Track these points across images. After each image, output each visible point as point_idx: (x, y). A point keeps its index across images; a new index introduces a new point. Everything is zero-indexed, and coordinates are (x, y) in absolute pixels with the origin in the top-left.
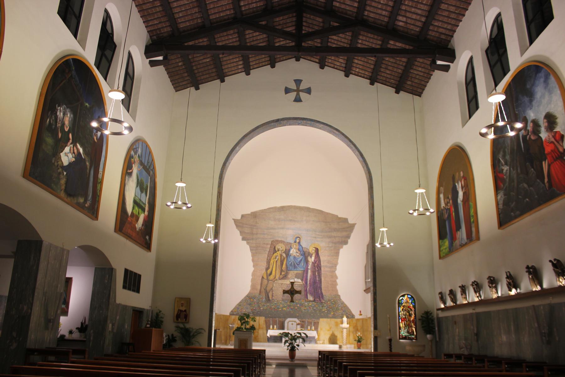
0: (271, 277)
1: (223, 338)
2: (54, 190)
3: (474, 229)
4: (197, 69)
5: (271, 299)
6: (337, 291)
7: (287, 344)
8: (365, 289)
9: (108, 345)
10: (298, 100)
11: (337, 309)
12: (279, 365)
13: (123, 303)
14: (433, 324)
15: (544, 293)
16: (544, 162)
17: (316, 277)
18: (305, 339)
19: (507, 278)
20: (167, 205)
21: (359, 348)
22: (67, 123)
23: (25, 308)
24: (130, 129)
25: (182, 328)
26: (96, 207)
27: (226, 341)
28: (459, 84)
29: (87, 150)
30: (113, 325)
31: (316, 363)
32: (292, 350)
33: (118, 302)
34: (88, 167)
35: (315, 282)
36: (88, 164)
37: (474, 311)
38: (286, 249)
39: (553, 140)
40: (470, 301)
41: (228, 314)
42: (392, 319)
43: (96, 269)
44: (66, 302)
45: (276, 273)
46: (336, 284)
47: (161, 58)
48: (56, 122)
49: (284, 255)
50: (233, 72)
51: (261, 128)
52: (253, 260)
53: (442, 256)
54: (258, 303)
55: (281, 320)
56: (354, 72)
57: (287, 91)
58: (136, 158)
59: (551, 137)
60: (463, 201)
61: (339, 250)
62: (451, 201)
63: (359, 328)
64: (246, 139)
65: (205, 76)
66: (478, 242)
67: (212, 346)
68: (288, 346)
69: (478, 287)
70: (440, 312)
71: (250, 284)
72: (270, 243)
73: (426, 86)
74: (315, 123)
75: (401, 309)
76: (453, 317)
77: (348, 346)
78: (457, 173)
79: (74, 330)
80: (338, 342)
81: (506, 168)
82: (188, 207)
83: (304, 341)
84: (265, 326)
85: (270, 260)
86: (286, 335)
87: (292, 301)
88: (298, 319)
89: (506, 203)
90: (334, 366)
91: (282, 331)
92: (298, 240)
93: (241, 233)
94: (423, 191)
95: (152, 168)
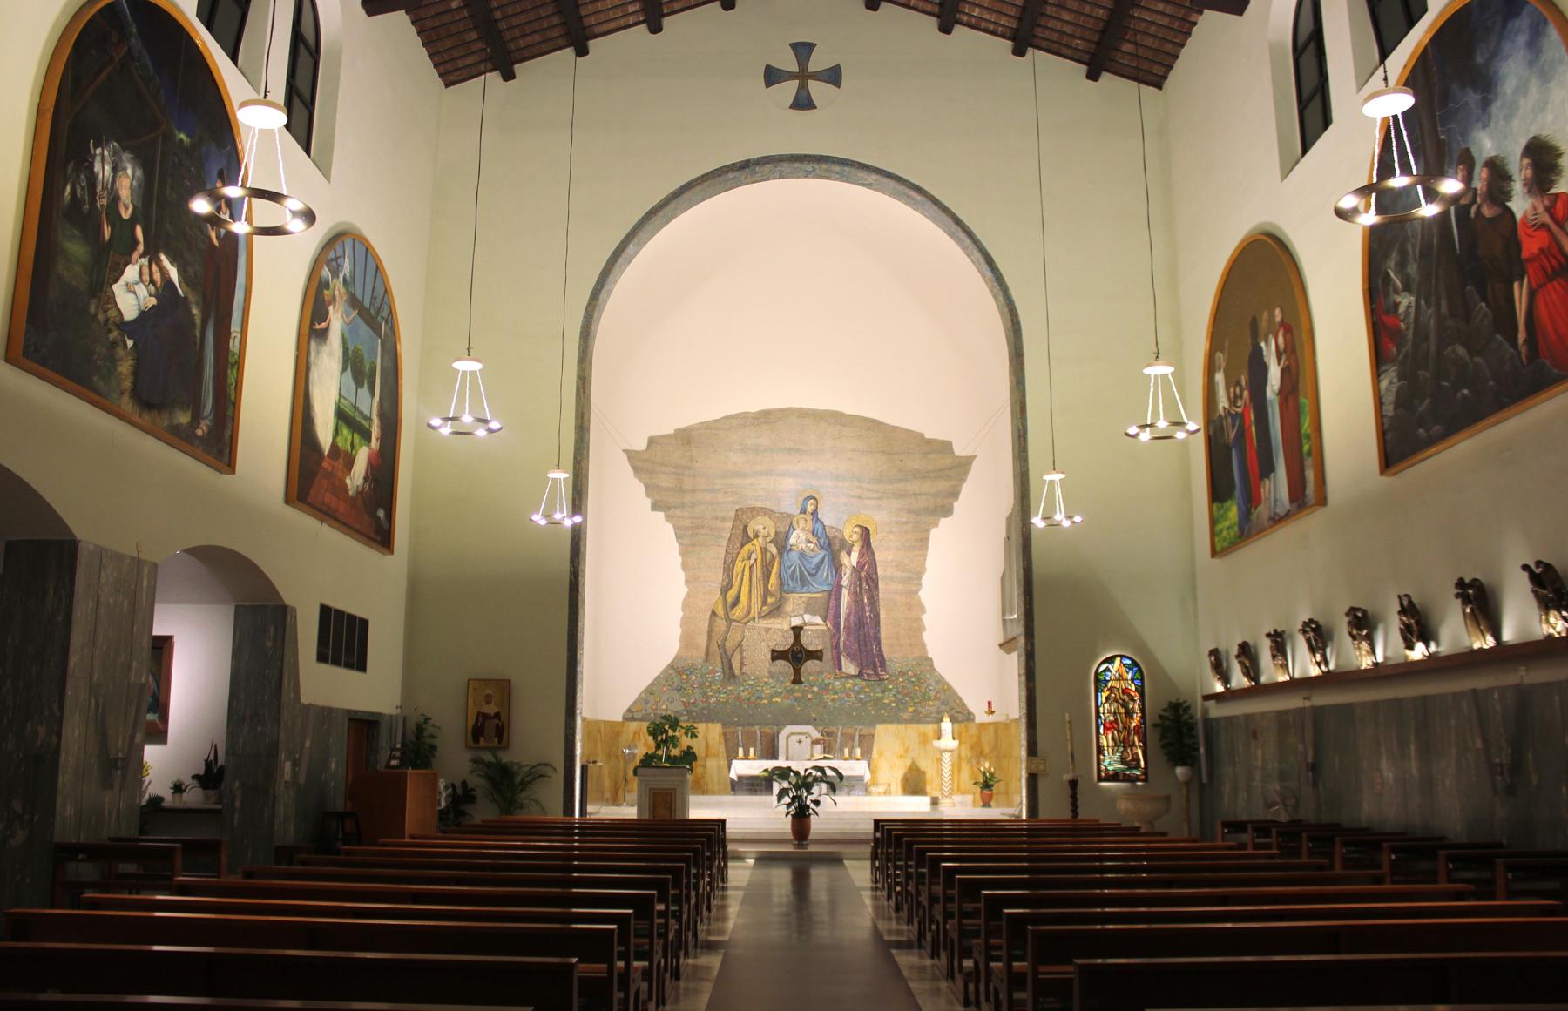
0: (738, 612)
1: (607, 783)
2: (100, 394)
3: (1310, 474)
4: (506, 17)
5: (737, 672)
6: (924, 645)
7: (787, 800)
8: (1001, 641)
9: (286, 824)
10: (803, 102)
11: (924, 698)
12: (765, 859)
14: (1194, 737)
15: (1504, 655)
16: (1516, 285)
17: (863, 609)
18: (836, 783)
19: (1403, 611)
20: (430, 426)
21: (986, 804)
22: (125, 194)
23: (42, 731)
24: (309, 216)
25: (489, 765)
26: (227, 435)
27: (616, 792)
28: (1274, 49)
29: (190, 269)
30: (295, 764)
31: (867, 850)
32: (801, 816)
33: (305, 699)
34: (198, 321)
36: (195, 311)
37: (1308, 704)
39: (1546, 218)
40: (1297, 676)
42: (1080, 749)
43: (237, 608)
44: (160, 705)
45: (751, 600)
46: (922, 628)
48: (93, 194)
49: (773, 549)
50: (613, 25)
51: (698, 188)
52: (685, 566)
53: (1218, 548)
54: (701, 685)
55: (767, 730)
56: (965, 18)
57: (772, 76)
58: (338, 287)
59: (1541, 209)
60: (1280, 393)
61: (928, 531)
62: (1246, 393)
63: (987, 749)
64: (656, 220)
65: (529, 40)
66: (1323, 509)
67: (577, 815)
68: (789, 805)
69: (1318, 636)
70: (1211, 703)
71: (678, 632)
73: (1176, 57)
74: (853, 170)
75: (1103, 697)
76: (1248, 717)
77: (957, 798)
78: (1265, 314)
79: (187, 781)
80: (928, 789)
81: (1405, 301)
82: (490, 431)
83: (833, 788)
84: (722, 748)
85: (733, 563)
86: (784, 773)
87: (797, 680)
88: (816, 726)
89: (1402, 401)
90: (918, 866)
91: (770, 764)
92: (811, 506)
93: (649, 489)
94: (1168, 370)
95: (385, 313)
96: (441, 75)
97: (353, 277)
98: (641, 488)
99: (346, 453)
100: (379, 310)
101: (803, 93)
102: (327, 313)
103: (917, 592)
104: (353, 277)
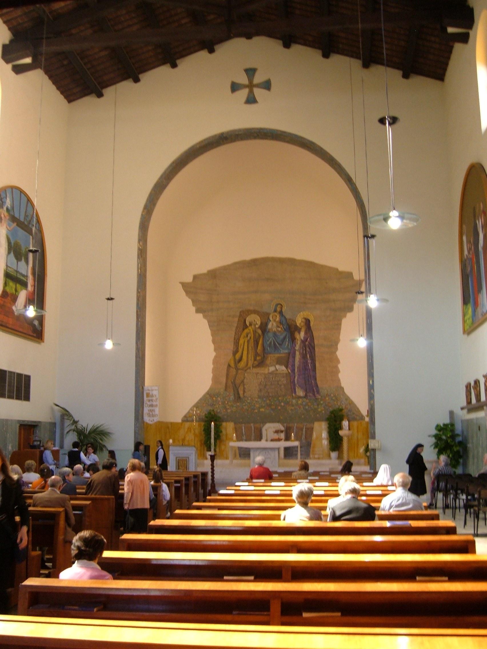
0: (242, 364)
5: (241, 396)
6: (339, 380)
10: (251, 100)
38: (261, 323)
47: (28, 60)
49: (260, 331)
52: (214, 342)
55: (257, 425)
57: (235, 87)
93: (194, 302)
97: (13, 208)
98: (190, 302)
99: (12, 295)
100: (30, 222)
103: (335, 352)
104: (13, 208)
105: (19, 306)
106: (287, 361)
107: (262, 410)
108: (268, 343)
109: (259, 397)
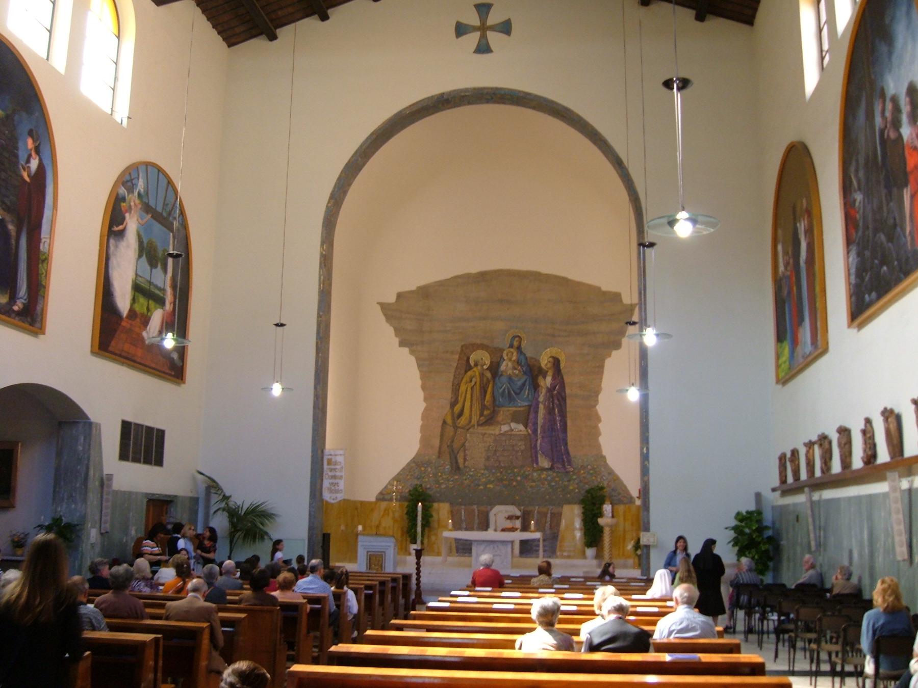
0: (463, 421)
5: (461, 466)
6: (599, 447)
10: (483, 48)
13: (125, 488)
34: (13, 233)
35: (552, 428)
41: (373, 499)
49: (489, 375)
52: (424, 388)
55: (483, 508)
57: (461, 30)
58: (133, 200)
61: (603, 361)
72: (459, 349)
85: (459, 385)
93: (398, 331)
96: (224, 39)
99: (142, 315)
100: (170, 214)
101: (484, 41)
102: (124, 219)
103: (595, 406)
105: (152, 331)
106: (526, 418)
107: (491, 486)
108: (501, 391)
109: (486, 468)
